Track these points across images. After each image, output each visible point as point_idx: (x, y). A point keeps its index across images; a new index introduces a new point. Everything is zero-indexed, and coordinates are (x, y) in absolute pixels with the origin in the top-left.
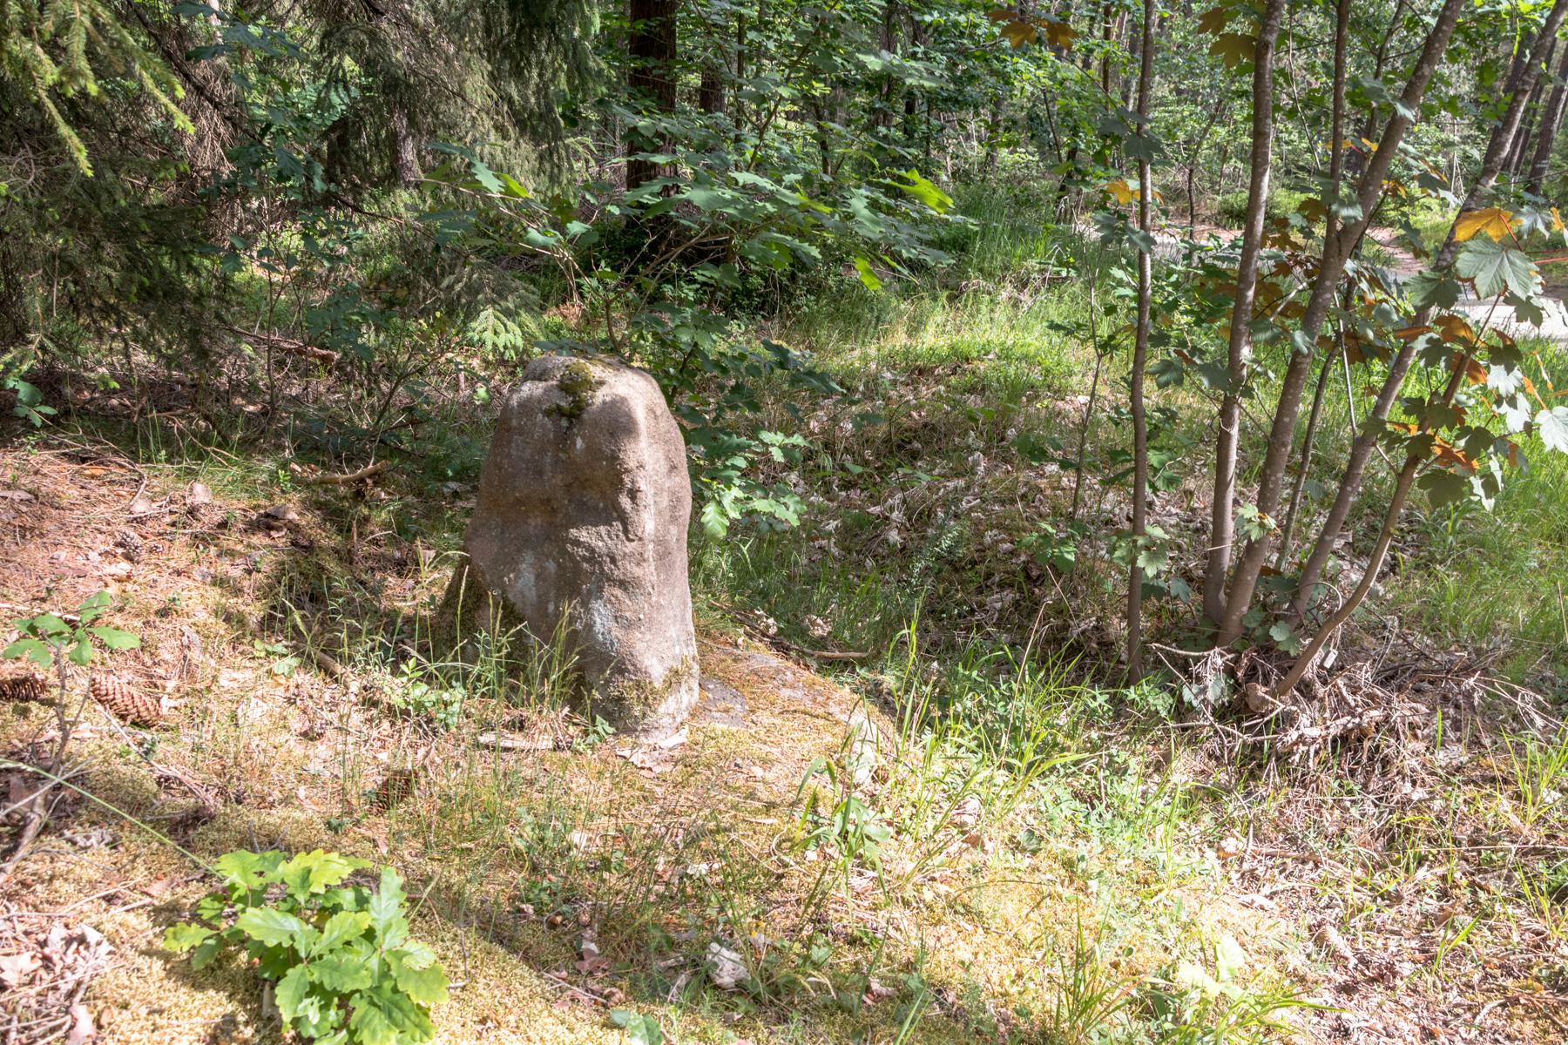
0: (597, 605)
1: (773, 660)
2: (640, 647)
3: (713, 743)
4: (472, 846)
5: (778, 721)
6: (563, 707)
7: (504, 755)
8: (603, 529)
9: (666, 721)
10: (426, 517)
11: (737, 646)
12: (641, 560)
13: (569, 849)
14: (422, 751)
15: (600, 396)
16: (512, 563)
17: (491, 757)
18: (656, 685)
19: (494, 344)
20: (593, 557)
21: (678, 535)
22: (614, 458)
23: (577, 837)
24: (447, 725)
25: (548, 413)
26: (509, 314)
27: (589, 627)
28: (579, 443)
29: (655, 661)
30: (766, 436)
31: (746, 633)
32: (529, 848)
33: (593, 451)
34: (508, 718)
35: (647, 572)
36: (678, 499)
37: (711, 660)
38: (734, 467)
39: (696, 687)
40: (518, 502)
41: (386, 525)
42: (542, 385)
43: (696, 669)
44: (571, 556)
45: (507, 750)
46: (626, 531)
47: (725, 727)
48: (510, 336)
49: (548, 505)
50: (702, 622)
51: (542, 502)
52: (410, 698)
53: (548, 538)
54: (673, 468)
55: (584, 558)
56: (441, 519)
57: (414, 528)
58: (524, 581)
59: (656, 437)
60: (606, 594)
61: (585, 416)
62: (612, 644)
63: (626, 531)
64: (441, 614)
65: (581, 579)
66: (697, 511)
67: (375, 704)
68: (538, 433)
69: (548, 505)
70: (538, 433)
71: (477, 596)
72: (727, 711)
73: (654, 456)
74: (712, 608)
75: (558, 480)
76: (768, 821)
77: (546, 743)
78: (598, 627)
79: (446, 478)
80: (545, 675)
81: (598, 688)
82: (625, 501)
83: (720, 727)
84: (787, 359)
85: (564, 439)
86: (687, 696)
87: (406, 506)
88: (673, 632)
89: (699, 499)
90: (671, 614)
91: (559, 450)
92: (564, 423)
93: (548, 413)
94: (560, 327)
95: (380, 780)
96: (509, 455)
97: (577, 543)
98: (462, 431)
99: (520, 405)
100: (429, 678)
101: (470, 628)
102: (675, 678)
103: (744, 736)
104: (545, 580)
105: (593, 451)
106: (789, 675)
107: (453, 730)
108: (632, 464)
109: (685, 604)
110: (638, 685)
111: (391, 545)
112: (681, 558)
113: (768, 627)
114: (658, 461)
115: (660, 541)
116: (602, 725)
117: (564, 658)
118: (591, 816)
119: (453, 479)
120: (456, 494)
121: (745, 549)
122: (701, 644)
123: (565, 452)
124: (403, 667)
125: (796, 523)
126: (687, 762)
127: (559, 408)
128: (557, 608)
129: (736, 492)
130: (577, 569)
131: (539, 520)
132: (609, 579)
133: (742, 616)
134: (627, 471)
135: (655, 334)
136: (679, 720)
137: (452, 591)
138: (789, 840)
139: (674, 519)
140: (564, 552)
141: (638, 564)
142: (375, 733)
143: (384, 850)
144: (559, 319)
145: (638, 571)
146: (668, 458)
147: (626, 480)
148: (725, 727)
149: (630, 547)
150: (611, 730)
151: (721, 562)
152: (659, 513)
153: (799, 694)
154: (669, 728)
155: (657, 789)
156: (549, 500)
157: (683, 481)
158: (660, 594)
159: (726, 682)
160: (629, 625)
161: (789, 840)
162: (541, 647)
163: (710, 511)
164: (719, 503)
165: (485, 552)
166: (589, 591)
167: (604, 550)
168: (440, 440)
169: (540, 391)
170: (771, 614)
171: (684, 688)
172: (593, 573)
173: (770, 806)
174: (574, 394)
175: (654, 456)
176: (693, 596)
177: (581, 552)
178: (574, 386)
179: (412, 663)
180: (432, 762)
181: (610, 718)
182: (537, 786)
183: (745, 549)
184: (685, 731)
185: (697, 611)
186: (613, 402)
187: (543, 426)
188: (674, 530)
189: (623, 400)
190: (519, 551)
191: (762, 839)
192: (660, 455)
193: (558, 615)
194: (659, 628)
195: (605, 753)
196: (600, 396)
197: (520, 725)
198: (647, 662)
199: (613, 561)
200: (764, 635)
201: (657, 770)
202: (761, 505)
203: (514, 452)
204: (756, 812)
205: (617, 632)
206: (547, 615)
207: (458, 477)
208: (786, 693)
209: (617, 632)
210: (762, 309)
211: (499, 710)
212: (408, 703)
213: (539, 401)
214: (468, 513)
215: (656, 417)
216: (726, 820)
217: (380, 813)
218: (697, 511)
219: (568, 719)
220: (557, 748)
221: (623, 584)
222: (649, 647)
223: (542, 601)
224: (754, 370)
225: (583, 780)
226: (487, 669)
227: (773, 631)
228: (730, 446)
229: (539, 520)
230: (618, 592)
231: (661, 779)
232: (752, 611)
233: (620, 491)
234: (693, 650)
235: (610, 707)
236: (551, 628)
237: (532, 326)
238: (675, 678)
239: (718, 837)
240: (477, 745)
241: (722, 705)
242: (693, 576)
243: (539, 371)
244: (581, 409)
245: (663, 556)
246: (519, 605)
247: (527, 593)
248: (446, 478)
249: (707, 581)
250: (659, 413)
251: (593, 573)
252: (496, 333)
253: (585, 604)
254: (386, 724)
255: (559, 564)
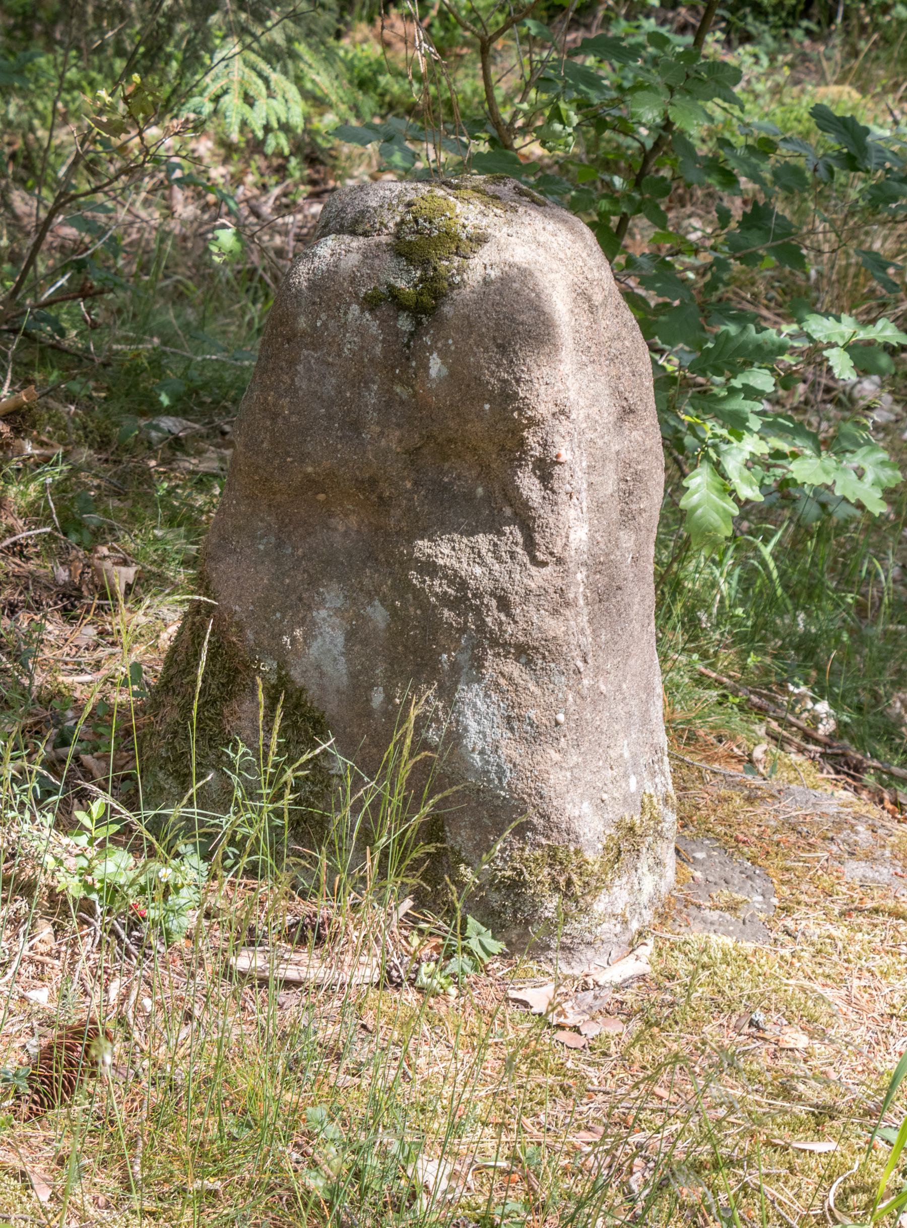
0: (470, 694)
1: (836, 797)
2: (557, 779)
3: (704, 975)
4: (218, 1185)
5: (840, 932)
6: (400, 898)
7: (282, 995)
8: (483, 541)
9: (609, 928)
10: (119, 494)
11: (750, 762)
12: (561, 603)
13: (413, 1196)
14: (115, 988)
15: (478, 268)
16: (299, 607)
17: (254, 998)
18: (589, 856)
19: (244, 123)
20: (463, 597)
21: (637, 552)
22: (507, 397)
23: (429, 1170)
24: (168, 933)
25: (371, 303)
26: (275, 55)
27: (455, 738)
28: (436, 366)
29: (586, 807)
30: (820, 327)
31: (774, 737)
32: (334, 1191)
33: (464, 382)
34: (289, 919)
35: (572, 628)
36: (638, 477)
37: (702, 795)
38: (751, 393)
39: (670, 859)
40: (312, 484)
41: (35, 514)
42: (357, 243)
43: (670, 820)
44: (418, 594)
45: (289, 984)
46: (530, 545)
47: (729, 942)
48: (277, 105)
49: (371, 491)
50: (679, 716)
51: (359, 484)
52: (94, 878)
53: (371, 557)
54: (627, 412)
55: (444, 599)
56: (147, 499)
57: (94, 519)
58: (323, 645)
59: (593, 351)
60: (489, 673)
61: (447, 310)
62: (501, 773)
63: (530, 545)
64: (156, 705)
65: (437, 641)
66: (675, 486)
67: (27, 889)
68: (350, 343)
69: (371, 491)
70: (350, 343)
71: (231, 675)
72: (733, 907)
73: (586, 388)
74: (700, 681)
75: (393, 441)
76: (820, 1147)
77: (368, 971)
78: (473, 739)
79: (155, 409)
80: (367, 838)
81: (473, 864)
82: (528, 484)
83: (721, 941)
84: (863, 149)
85: (404, 357)
86: (652, 879)
87: (75, 470)
88: (624, 748)
89: (679, 455)
90: (620, 710)
91: (394, 379)
92: (404, 323)
93: (371, 303)
94: (379, 68)
95: (34, 1045)
96: (292, 390)
97: (430, 568)
98: (179, 297)
99: (314, 286)
100: (125, 837)
101: (215, 737)
102: (626, 843)
103: (769, 964)
104: (365, 642)
105: (464, 382)
106: (863, 834)
107: (180, 941)
108: (543, 409)
109: (649, 689)
110: (553, 856)
111: (50, 554)
112: (641, 598)
113: (816, 719)
114: (595, 399)
115: (600, 564)
116: (480, 937)
117: (411, 806)
118: (455, 1129)
119: (169, 412)
120: (176, 444)
121: (767, 551)
122: (679, 764)
123: (407, 383)
124: (80, 815)
125: (878, 507)
126: (649, 1011)
127: (394, 294)
128: (389, 698)
129: (752, 445)
130: (430, 623)
131: (353, 520)
132: (494, 643)
133: (761, 699)
134: (533, 422)
135: (582, 106)
136: (635, 926)
137: (180, 659)
138: (865, 1189)
139: (628, 518)
140: (403, 587)
141: (555, 612)
142: (23, 947)
143: (44, 1194)
144: (374, 50)
145: (554, 627)
146: (618, 393)
147: (532, 439)
148: (729, 942)
149: (538, 577)
150: (497, 947)
151: (716, 579)
152: (599, 507)
153: (884, 873)
154: (613, 949)
155: (591, 1072)
156: (373, 482)
157: (647, 435)
158: (598, 671)
159: (731, 845)
160: (535, 736)
161: (865, 1189)
162: (358, 783)
163: (699, 481)
164: (718, 468)
165: (243, 584)
166: (455, 667)
167: (487, 584)
168: (143, 326)
169: (354, 259)
170: (821, 691)
171: (644, 864)
172: (463, 630)
173: (823, 1114)
174: (425, 263)
175: (586, 388)
176: (664, 658)
177: (440, 586)
178: (421, 245)
179: (96, 808)
180: (139, 1009)
181: (494, 921)
182: (346, 1063)
183: (767, 551)
184: (646, 951)
185: (670, 689)
186: (505, 280)
187: (361, 332)
188: (627, 540)
189: (525, 274)
190: (313, 582)
191: (809, 1184)
192: (602, 387)
193: (393, 716)
194: (597, 740)
195: (488, 996)
196: (478, 268)
197: (308, 934)
198: (572, 811)
199: (504, 604)
200: (808, 737)
201: (591, 1030)
202: (808, 470)
203: (302, 384)
204: (796, 1126)
205: (510, 750)
206: (369, 713)
207: (179, 409)
208: (855, 870)
209: (510, 750)
210: (806, 15)
211: (274, 902)
212: (90, 888)
213: (353, 280)
214: (202, 482)
215: (592, 309)
216: (731, 1144)
217: (34, 1115)
218: (675, 486)
219: (411, 922)
220: (389, 981)
221: (523, 653)
222: (575, 781)
223: (359, 686)
224: (790, 179)
225: (439, 1051)
226: (250, 820)
227: (825, 728)
228: (741, 349)
229: (353, 520)
230: (513, 668)
231: (597, 1050)
232: (782, 686)
233: (519, 463)
234: (665, 783)
235: (495, 899)
236: (380, 741)
237: (322, 79)
238: (626, 843)
239: (719, 1180)
240: (228, 973)
241: (724, 895)
242: (663, 611)
243: (350, 214)
244: (438, 296)
245: (606, 596)
246: (313, 692)
247: (328, 669)
248: (155, 409)
249: (691, 624)
250: (598, 298)
251: (463, 630)
252: (249, 100)
253: (447, 693)
254: (45, 930)
255: (394, 613)
